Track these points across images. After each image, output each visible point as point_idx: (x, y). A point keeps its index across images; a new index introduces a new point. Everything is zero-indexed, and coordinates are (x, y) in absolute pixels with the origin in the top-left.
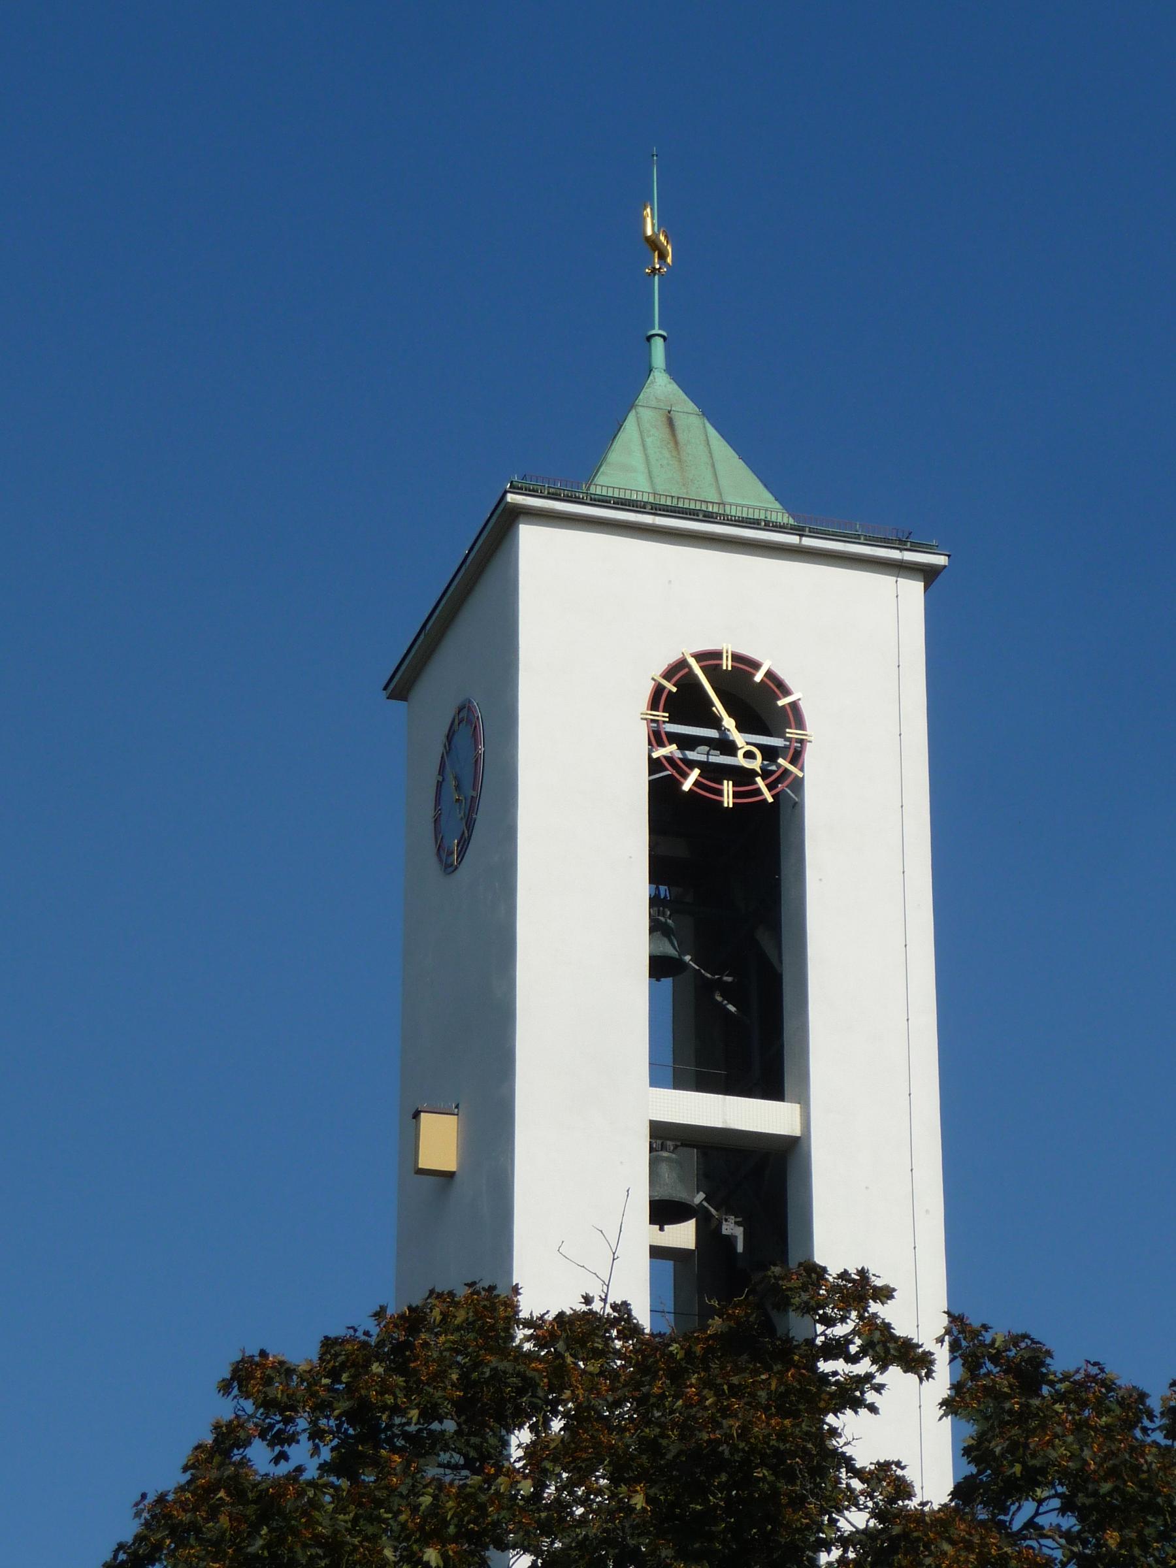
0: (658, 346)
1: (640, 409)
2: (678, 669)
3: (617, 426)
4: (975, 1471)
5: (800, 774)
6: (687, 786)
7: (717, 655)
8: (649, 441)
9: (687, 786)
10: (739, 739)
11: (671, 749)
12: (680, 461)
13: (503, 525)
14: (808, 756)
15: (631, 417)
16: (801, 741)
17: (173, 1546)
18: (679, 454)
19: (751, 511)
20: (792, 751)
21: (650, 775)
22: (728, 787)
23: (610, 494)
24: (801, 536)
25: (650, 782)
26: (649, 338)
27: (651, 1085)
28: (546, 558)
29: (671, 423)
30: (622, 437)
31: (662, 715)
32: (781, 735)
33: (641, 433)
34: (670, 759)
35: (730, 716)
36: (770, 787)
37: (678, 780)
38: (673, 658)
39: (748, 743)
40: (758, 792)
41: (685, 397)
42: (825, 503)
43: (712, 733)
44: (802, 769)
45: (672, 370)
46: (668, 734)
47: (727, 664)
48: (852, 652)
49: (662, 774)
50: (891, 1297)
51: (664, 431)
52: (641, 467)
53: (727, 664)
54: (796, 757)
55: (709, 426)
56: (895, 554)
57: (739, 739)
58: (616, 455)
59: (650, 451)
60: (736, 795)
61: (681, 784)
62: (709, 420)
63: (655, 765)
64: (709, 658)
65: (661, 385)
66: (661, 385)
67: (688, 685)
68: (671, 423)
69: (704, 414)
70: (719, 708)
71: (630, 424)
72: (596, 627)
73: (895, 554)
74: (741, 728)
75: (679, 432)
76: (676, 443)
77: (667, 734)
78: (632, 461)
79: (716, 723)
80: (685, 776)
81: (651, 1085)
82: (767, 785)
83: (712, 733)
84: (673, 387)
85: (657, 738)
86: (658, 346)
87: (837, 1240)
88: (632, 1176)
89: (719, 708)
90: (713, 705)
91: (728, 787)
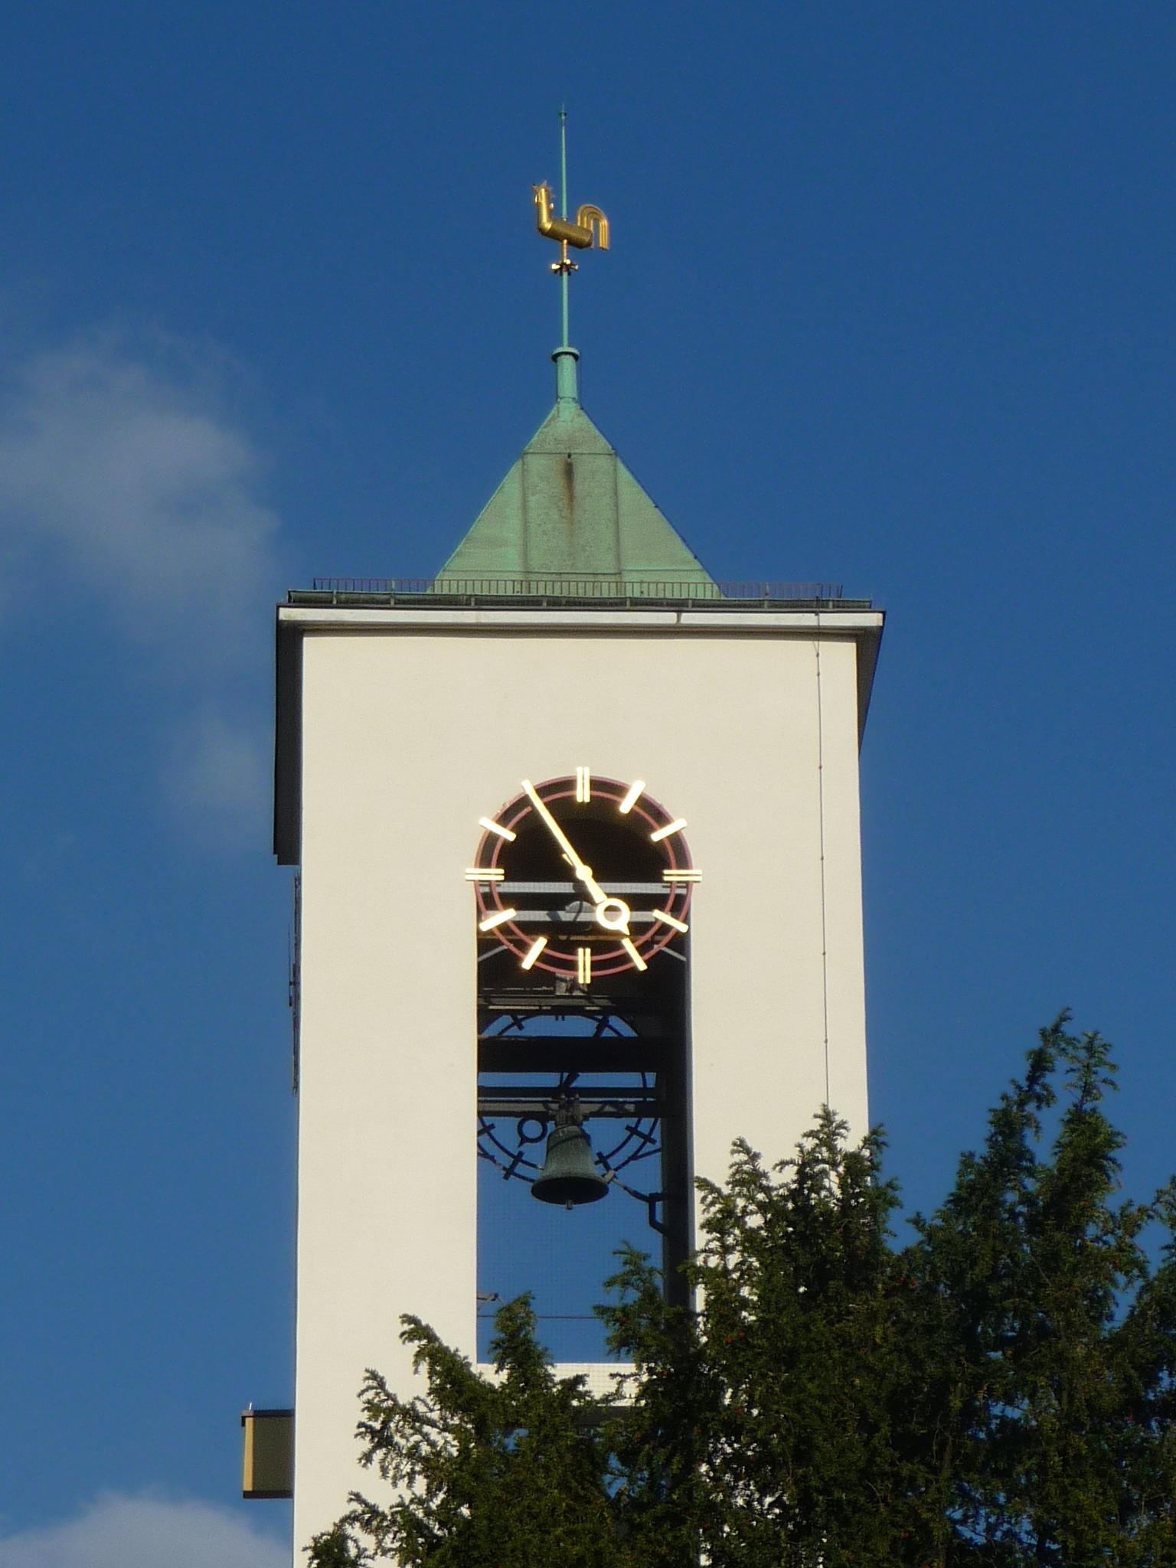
0: (567, 366)
1: (529, 458)
2: (517, 812)
5: (682, 928)
6: (528, 962)
7: (568, 784)
8: (533, 500)
9: (528, 962)
10: (595, 889)
11: (508, 915)
12: (572, 522)
14: (696, 904)
15: (515, 471)
16: (687, 885)
19: (486, 584)
20: (672, 898)
21: (479, 955)
22: (584, 957)
23: (541, 592)
24: (679, 612)
25: (480, 964)
26: (555, 358)
29: (569, 471)
30: (497, 499)
31: (495, 874)
32: (657, 878)
34: (504, 928)
35: (585, 861)
36: (642, 950)
37: (515, 955)
38: (509, 798)
39: (609, 895)
40: (626, 958)
41: (597, 433)
42: (754, 566)
43: (565, 888)
44: (686, 920)
45: (585, 401)
46: (503, 896)
47: (583, 794)
49: (497, 950)
50: (405, 1316)
51: (559, 482)
53: (583, 794)
54: (679, 906)
55: (624, 474)
56: (808, 620)
57: (595, 889)
58: (482, 527)
60: (595, 966)
61: (519, 960)
62: (624, 462)
63: (485, 942)
64: (557, 791)
65: (567, 418)
66: (567, 418)
67: (531, 830)
68: (569, 471)
69: (616, 452)
70: (570, 855)
71: (511, 484)
72: (418, 751)
73: (808, 620)
74: (598, 877)
76: (571, 497)
77: (501, 895)
78: (501, 539)
79: (566, 873)
80: (524, 947)
82: (638, 948)
83: (565, 888)
84: (584, 420)
85: (488, 901)
86: (567, 366)
89: (570, 855)
90: (559, 850)
91: (584, 957)
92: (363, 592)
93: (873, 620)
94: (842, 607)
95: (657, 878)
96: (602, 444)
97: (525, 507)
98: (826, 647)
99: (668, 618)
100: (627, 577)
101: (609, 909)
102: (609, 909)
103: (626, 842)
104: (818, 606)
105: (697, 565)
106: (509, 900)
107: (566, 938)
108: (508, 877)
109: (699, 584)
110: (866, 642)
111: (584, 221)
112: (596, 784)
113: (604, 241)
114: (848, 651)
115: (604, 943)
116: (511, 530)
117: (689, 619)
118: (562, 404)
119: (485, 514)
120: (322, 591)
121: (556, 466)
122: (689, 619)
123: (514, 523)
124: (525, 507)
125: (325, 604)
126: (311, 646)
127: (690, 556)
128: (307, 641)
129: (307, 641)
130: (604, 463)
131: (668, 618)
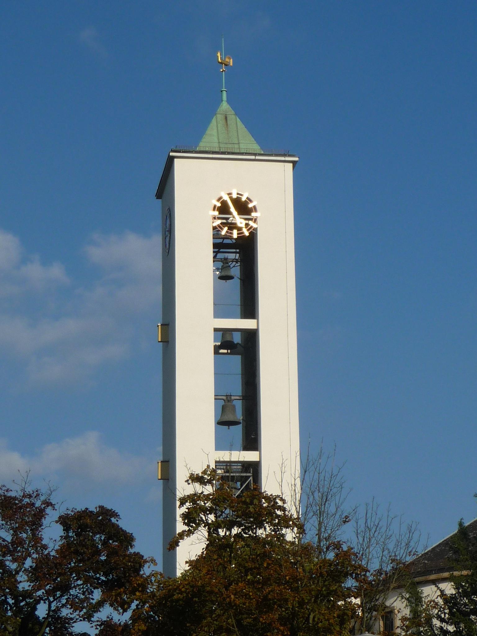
0: (224, 93)
3: (209, 122)
4: (292, 509)
13: (170, 162)
15: (215, 118)
17: (75, 578)
18: (228, 134)
26: (222, 91)
27: (216, 450)
28: (185, 170)
29: (226, 118)
30: (211, 125)
32: (250, 215)
33: (217, 122)
45: (228, 101)
48: (269, 190)
51: (224, 121)
52: (215, 134)
55: (238, 119)
56: (283, 159)
59: (219, 128)
63: (214, 228)
65: (225, 106)
66: (225, 106)
68: (226, 118)
69: (236, 114)
71: (214, 121)
72: (201, 187)
73: (283, 159)
74: (239, 214)
75: (228, 120)
76: (227, 125)
81: (216, 450)
84: (228, 106)
86: (224, 93)
87: (269, 486)
88: (209, 343)
92: (188, 149)
93: (296, 159)
94: (290, 156)
95: (250, 215)
96: (233, 112)
97: (217, 127)
98: (286, 164)
99: (253, 157)
100: (240, 145)
101: (240, 221)
102: (240, 221)
103: (243, 208)
104: (284, 155)
105: (255, 142)
106: (219, 218)
107: (232, 226)
108: (219, 214)
109: (256, 148)
110: (294, 163)
111: (227, 60)
112: (255, 207)
113: (231, 64)
114: (291, 165)
115: (239, 229)
116: (214, 132)
117: (257, 158)
118: (223, 102)
119: (209, 129)
120: (178, 149)
121: (223, 117)
122: (257, 158)
123: (215, 130)
124: (217, 127)
125: (179, 152)
126: (176, 160)
127: (253, 140)
128: (175, 160)
129: (175, 160)
130: (234, 117)
131: (253, 157)
